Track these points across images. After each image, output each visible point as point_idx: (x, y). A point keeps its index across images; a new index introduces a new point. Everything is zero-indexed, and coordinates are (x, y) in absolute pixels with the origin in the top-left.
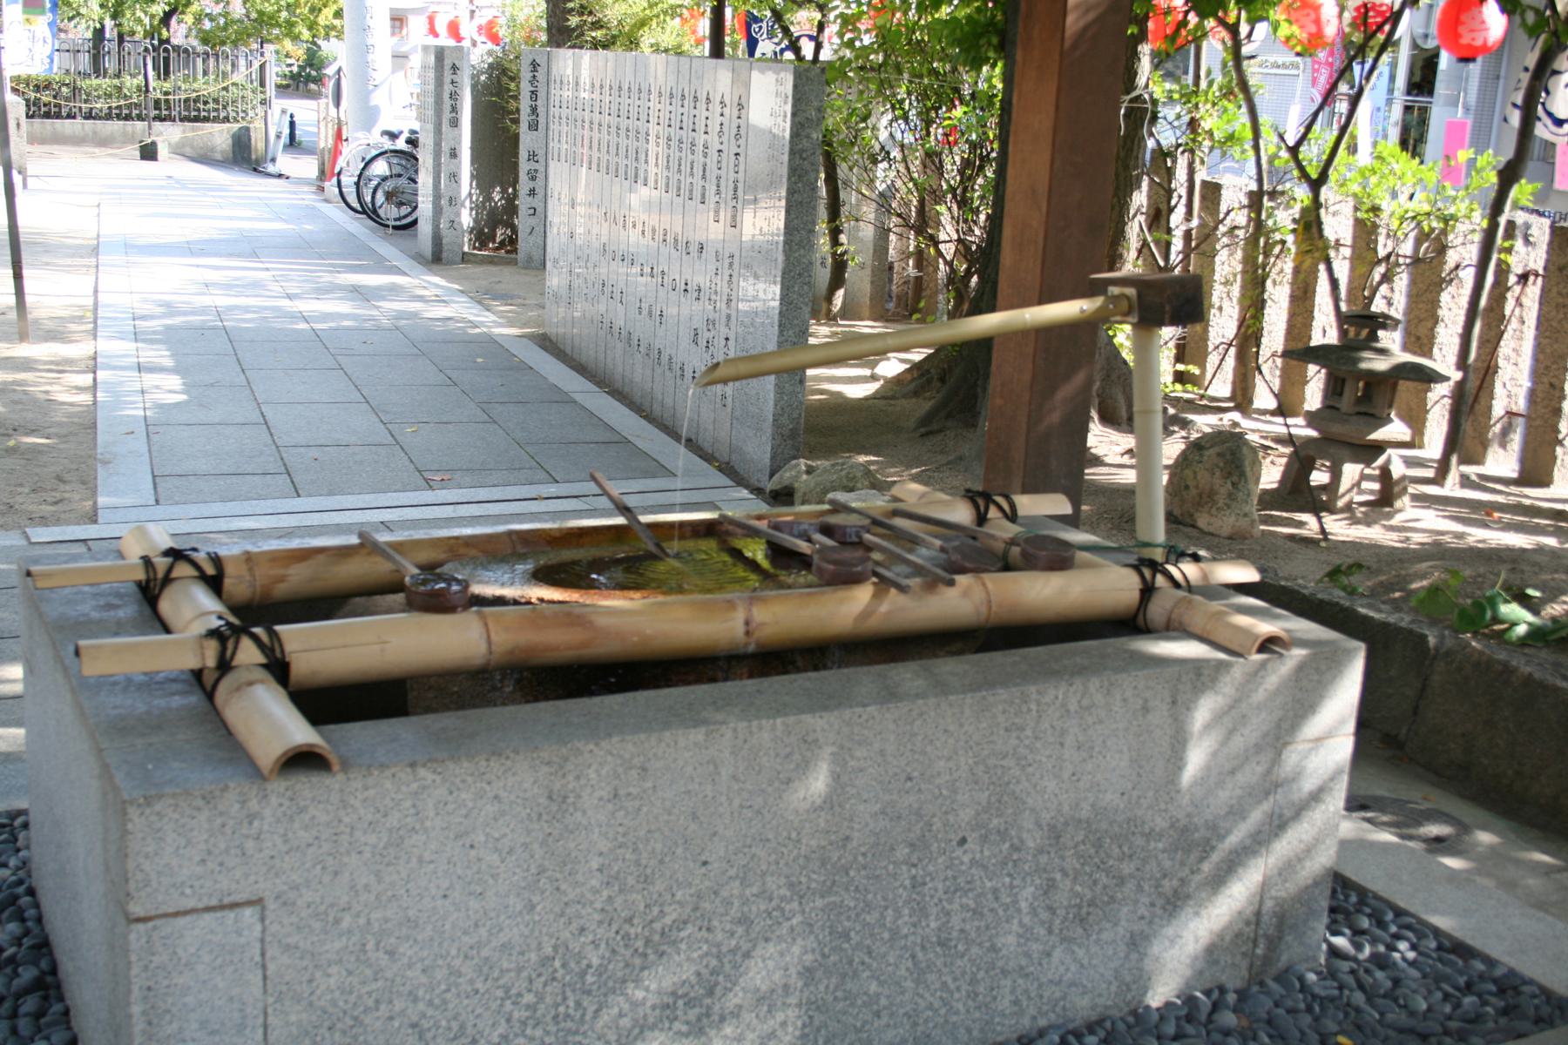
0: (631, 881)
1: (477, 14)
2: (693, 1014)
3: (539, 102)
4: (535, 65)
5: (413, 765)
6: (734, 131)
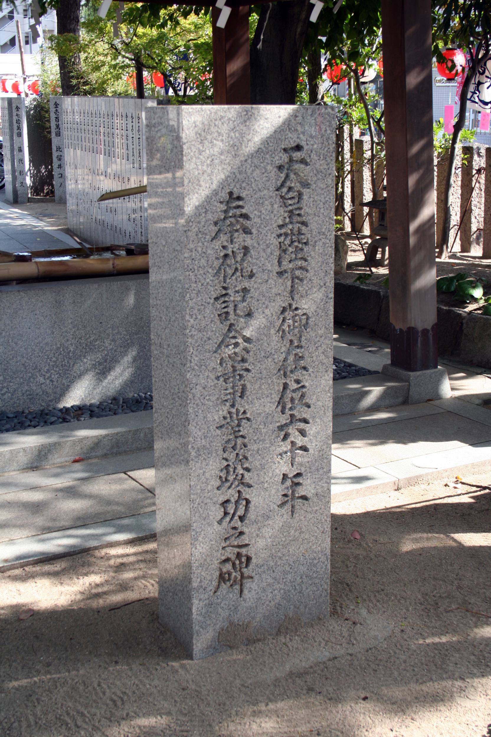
0: (80, 327)
1: (27, 79)
2: (101, 367)
4: (56, 105)
5: (19, 291)
6: (137, 129)
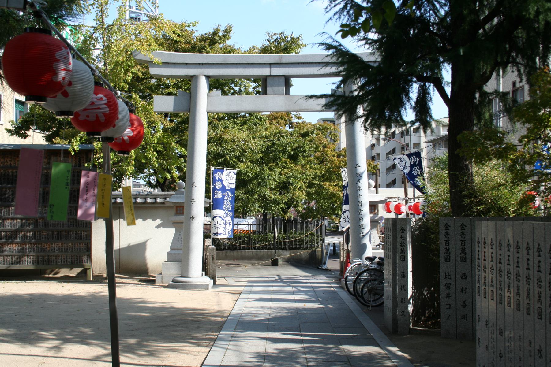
3: (450, 246)
